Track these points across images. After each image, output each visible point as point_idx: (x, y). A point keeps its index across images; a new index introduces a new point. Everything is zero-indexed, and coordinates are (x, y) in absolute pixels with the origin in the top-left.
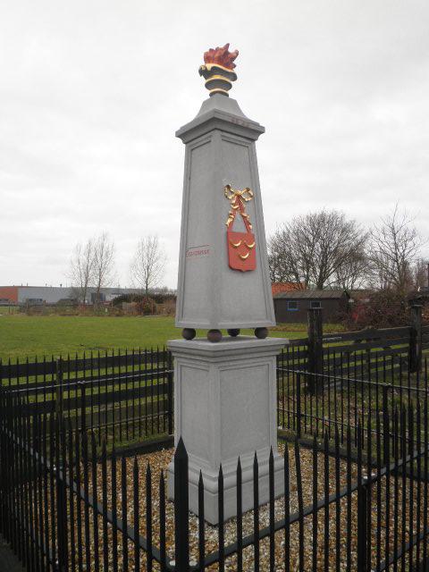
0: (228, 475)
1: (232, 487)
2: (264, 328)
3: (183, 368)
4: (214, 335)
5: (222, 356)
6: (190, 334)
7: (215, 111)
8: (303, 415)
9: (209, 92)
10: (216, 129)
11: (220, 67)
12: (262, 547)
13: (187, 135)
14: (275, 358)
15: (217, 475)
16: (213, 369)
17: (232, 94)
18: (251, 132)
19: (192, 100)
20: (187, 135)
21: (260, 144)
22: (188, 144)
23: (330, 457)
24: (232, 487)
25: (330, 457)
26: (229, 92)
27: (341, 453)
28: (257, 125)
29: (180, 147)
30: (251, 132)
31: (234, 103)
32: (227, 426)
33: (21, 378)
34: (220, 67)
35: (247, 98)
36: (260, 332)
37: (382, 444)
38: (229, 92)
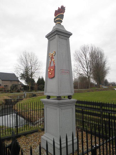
0: (63, 144)
1: (65, 147)
2: (71, 96)
3: (47, 108)
4: (59, 98)
5: (62, 105)
6: (49, 97)
7: (57, 28)
8: (84, 122)
9: (55, 24)
10: (57, 34)
11: (60, 13)
12: (6, 110)
13: (48, 36)
14: (75, 105)
15: (53, 140)
16: (58, 109)
17: (62, 24)
18: (68, 35)
19: (51, 26)
20: (48, 36)
21: (71, 38)
22: (49, 40)
23: (92, 135)
24: (65, 147)
25: (92, 135)
26: (61, 23)
27: (104, 136)
28: (70, 32)
29: (47, 40)
30: (68, 35)
31: (63, 26)
32: (59, 126)
33: (98, 106)
34: (60, 13)
35: (67, 24)
36: (70, 97)
37: (111, 131)
38: (61, 23)
